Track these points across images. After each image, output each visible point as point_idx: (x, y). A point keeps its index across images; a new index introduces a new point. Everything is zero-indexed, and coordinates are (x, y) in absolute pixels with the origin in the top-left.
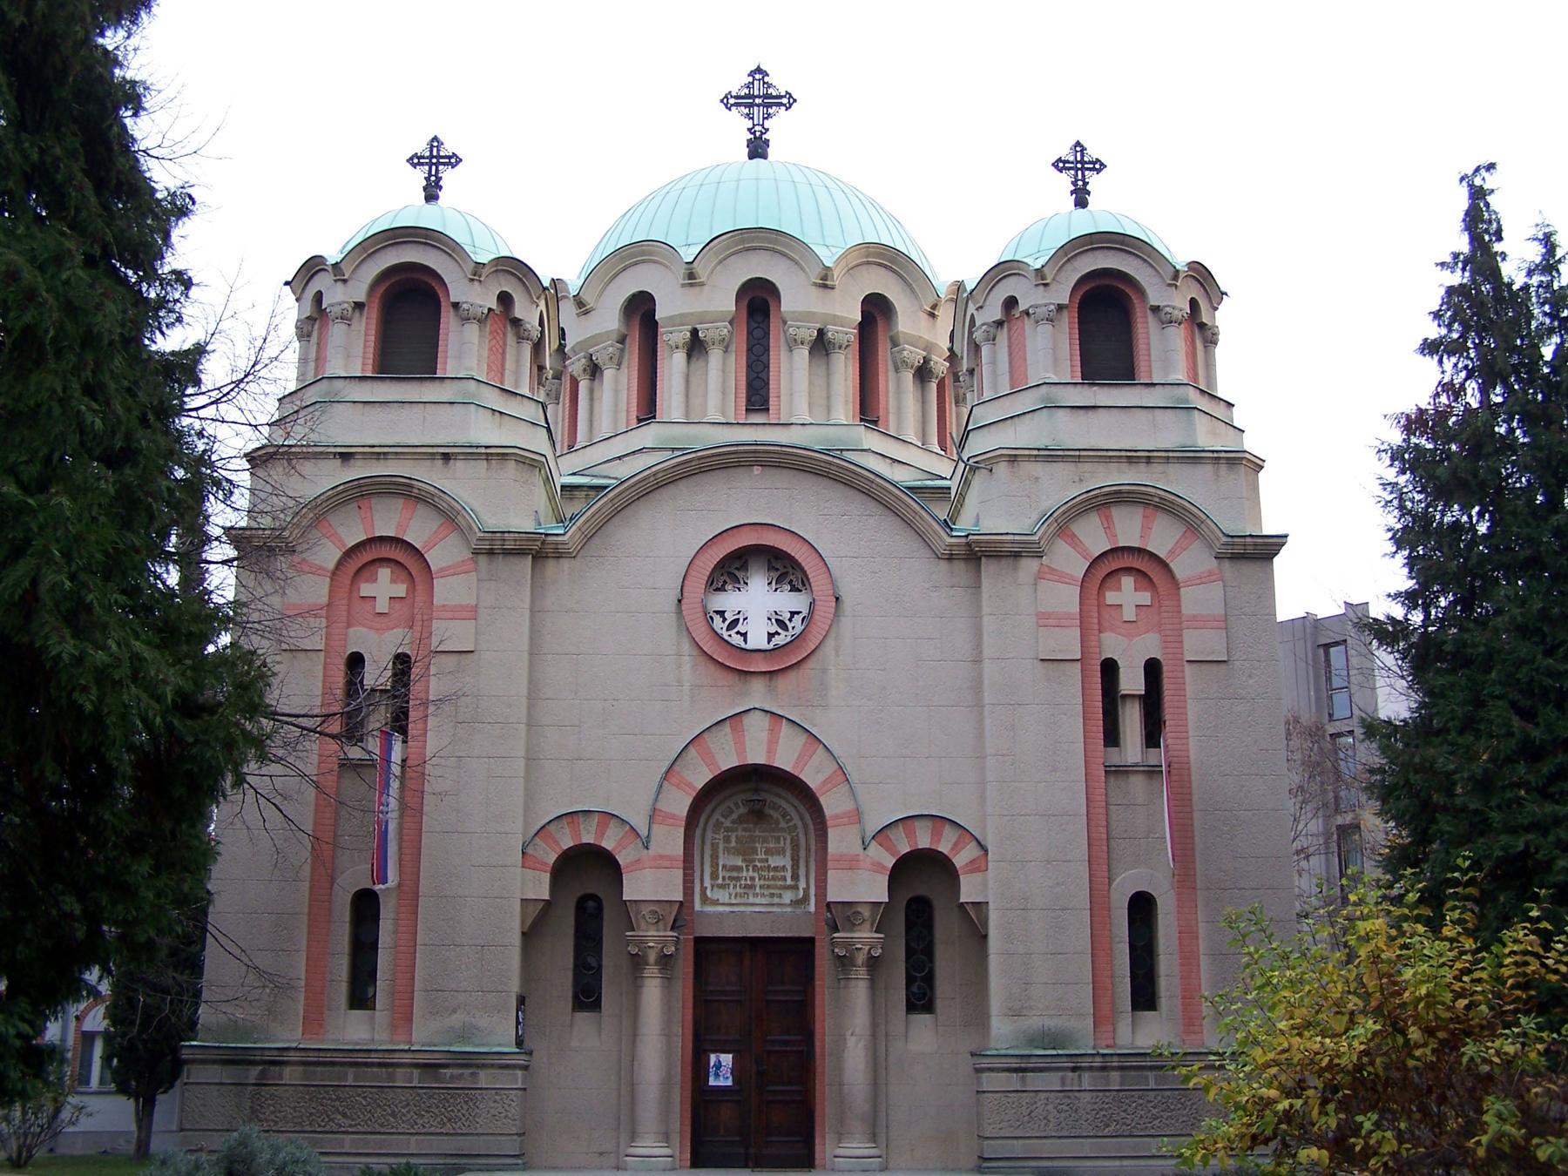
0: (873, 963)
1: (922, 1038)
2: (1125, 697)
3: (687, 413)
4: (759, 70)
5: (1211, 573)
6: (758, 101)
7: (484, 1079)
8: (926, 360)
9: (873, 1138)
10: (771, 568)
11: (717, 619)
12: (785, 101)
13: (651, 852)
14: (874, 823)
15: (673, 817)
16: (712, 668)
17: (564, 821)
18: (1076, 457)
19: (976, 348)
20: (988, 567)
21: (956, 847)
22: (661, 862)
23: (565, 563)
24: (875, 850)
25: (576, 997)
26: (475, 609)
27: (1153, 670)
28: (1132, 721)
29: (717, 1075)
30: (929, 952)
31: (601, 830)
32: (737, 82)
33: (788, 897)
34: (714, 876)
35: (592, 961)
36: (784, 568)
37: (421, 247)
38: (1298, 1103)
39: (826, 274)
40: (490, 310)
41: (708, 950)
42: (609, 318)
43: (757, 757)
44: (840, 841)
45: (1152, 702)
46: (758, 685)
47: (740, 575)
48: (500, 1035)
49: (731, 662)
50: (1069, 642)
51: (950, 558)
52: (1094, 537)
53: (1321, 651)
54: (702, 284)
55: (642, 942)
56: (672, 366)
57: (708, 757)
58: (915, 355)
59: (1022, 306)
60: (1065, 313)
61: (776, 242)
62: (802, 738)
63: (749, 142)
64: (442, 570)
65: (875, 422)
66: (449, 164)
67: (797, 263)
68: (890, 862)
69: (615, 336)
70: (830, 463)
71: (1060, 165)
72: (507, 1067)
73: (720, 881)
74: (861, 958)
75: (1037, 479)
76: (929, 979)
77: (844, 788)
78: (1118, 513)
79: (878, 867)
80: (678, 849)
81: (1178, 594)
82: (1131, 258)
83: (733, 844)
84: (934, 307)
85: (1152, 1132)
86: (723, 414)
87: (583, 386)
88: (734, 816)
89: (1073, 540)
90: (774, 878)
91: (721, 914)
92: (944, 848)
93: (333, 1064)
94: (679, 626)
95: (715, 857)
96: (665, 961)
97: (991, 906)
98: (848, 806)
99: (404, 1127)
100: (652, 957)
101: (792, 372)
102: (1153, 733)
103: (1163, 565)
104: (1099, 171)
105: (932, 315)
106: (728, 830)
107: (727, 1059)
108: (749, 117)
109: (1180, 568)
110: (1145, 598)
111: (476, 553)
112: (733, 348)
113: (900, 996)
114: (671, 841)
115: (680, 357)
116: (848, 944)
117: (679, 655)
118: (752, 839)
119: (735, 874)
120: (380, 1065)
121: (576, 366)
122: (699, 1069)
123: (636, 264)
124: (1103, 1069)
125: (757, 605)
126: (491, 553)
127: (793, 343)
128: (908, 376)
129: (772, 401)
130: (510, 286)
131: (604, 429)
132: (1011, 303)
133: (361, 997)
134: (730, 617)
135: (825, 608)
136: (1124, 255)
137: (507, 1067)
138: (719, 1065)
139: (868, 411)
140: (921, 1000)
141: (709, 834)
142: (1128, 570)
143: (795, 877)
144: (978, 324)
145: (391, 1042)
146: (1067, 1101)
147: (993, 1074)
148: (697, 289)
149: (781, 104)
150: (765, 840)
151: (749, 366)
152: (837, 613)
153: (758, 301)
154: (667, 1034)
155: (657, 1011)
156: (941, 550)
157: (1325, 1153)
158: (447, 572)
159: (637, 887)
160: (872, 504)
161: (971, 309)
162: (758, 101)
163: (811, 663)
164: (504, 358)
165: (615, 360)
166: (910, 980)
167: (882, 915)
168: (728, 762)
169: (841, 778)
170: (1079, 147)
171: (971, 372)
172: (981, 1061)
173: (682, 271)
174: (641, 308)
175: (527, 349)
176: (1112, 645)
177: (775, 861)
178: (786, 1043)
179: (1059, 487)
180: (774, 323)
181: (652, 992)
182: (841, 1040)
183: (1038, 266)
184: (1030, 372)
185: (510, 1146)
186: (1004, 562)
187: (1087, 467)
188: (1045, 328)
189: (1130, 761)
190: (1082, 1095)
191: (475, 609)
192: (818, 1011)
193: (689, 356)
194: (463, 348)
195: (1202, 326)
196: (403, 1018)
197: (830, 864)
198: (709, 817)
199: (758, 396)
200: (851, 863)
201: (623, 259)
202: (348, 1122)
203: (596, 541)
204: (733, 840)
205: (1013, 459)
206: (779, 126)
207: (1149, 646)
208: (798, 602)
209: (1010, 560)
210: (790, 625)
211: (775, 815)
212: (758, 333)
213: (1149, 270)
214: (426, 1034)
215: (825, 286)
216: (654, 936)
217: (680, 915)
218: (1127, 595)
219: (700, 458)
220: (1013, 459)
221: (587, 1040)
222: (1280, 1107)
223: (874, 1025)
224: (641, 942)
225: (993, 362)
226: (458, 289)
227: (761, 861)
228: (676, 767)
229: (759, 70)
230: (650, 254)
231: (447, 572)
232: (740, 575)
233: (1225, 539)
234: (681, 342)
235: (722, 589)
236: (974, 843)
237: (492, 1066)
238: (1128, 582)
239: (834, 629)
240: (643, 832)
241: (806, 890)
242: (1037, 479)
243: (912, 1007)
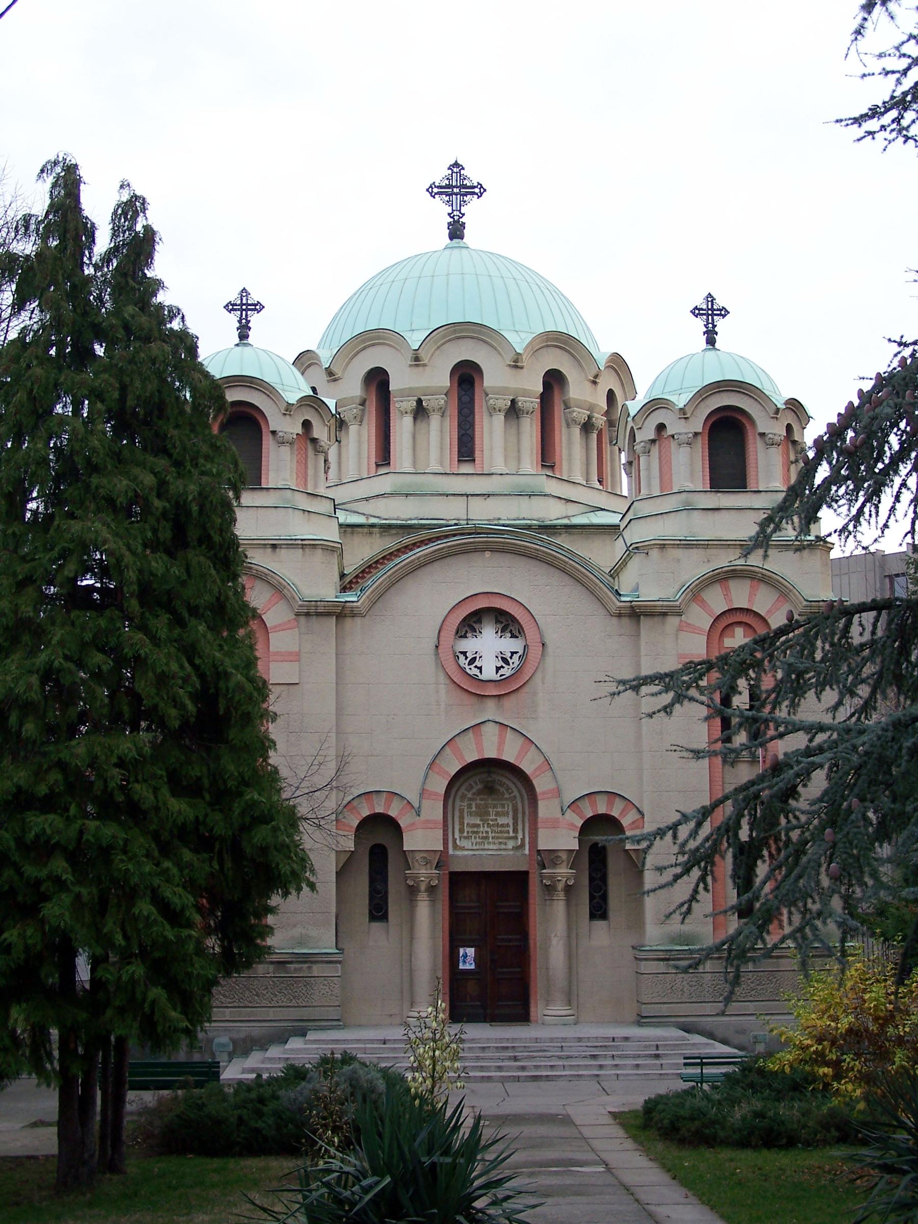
0: (568, 889)
1: (600, 936)
4: (456, 164)
6: (455, 190)
7: (317, 970)
8: (590, 417)
9: (569, 1003)
11: (462, 657)
12: (477, 190)
13: (422, 818)
14: (569, 798)
15: (436, 794)
16: (459, 692)
20: (645, 622)
21: (624, 812)
22: (428, 825)
23: (358, 620)
24: (570, 815)
25: (370, 912)
26: (298, 654)
29: (464, 962)
30: (604, 879)
31: (388, 804)
32: (439, 174)
33: (511, 844)
34: (461, 831)
36: (507, 622)
37: (248, 389)
38: (820, 1047)
39: (517, 358)
41: (459, 881)
43: (491, 753)
44: (546, 809)
46: (491, 704)
47: (476, 626)
48: (326, 943)
49: (472, 688)
51: (620, 616)
52: (717, 600)
53: (887, 580)
54: (425, 365)
55: (416, 877)
56: (402, 426)
57: (458, 754)
58: (581, 415)
59: (670, 431)
60: (699, 438)
61: (480, 332)
62: (521, 740)
63: (449, 224)
64: (275, 627)
66: (255, 309)
67: (495, 349)
68: (579, 823)
69: (358, 401)
70: (538, 550)
72: (331, 962)
73: (465, 834)
74: (560, 886)
75: (679, 560)
76: (605, 897)
77: (549, 774)
78: (732, 584)
79: (572, 826)
82: (746, 398)
83: (474, 809)
84: (596, 376)
85: (751, 999)
86: (442, 465)
88: (474, 790)
89: (703, 604)
90: (501, 832)
91: (466, 856)
92: (615, 813)
94: (437, 664)
95: (462, 818)
96: (431, 889)
98: (553, 786)
99: (265, 1003)
100: (423, 887)
101: (491, 431)
104: (724, 316)
105: (594, 383)
106: (470, 799)
107: (471, 951)
111: (298, 615)
112: (448, 413)
113: (585, 910)
114: (434, 810)
115: (408, 420)
116: (552, 877)
117: (437, 683)
118: (486, 806)
119: (475, 829)
122: (453, 958)
123: (373, 345)
125: (489, 646)
126: (307, 614)
127: (492, 411)
128: (576, 431)
129: (477, 454)
130: (310, 415)
131: (351, 472)
132: (661, 427)
135: (535, 651)
136: (742, 396)
137: (331, 962)
138: (465, 956)
139: (547, 457)
140: (599, 911)
141: (458, 803)
142: (739, 623)
143: (515, 830)
146: (695, 979)
147: (648, 962)
148: (421, 369)
149: (474, 193)
150: (495, 806)
151: (459, 425)
152: (543, 654)
153: (466, 376)
154: (433, 937)
155: (427, 921)
157: (831, 1070)
158: (278, 628)
160: (567, 578)
162: (455, 190)
163: (526, 689)
164: (306, 468)
165: (358, 419)
166: (592, 898)
167: (574, 858)
170: (710, 298)
172: (639, 952)
173: (410, 355)
177: (502, 820)
178: (510, 940)
179: (695, 567)
181: (423, 909)
182: (547, 940)
183: (681, 406)
184: (675, 479)
186: (656, 619)
187: (714, 551)
188: (685, 449)
190: (706, 975)
191: (298, 654)
192: (531, 920)
195: (794, 442)
197: (539, 825)
198: (457, 791)
200: (554, 824)
201: (364, 341)
202: (228, 1000)
203: (379, 605)
204: (474, 806)
205: (663, 547)
206: (473, 210)
208: (516, 645)
210: (511, 661)
211: (502, 790)
212: (466, 399)
215: (516, 367)
216: (424, 873)
217: (441, 860)
219: (449, 547)
220: (663, 547)
221: (379, 941)
222: (812, 1049)
223: (569, 928)
224: (415, 878)
225: (648, 469)
227: (492, 820)
228: (437, 761)
229: (456, 164)
230: (384, 338)
231: (278, 628)
232: (476, 626)
233: (805, 603)
234: (409, 409)
235: (465, 636)
236: (635, 810)
237: (322, 962)
239: (541, 665)
240: (416, 805)
241: (523, 840)
242: (679, 560)
243: (593, 916)
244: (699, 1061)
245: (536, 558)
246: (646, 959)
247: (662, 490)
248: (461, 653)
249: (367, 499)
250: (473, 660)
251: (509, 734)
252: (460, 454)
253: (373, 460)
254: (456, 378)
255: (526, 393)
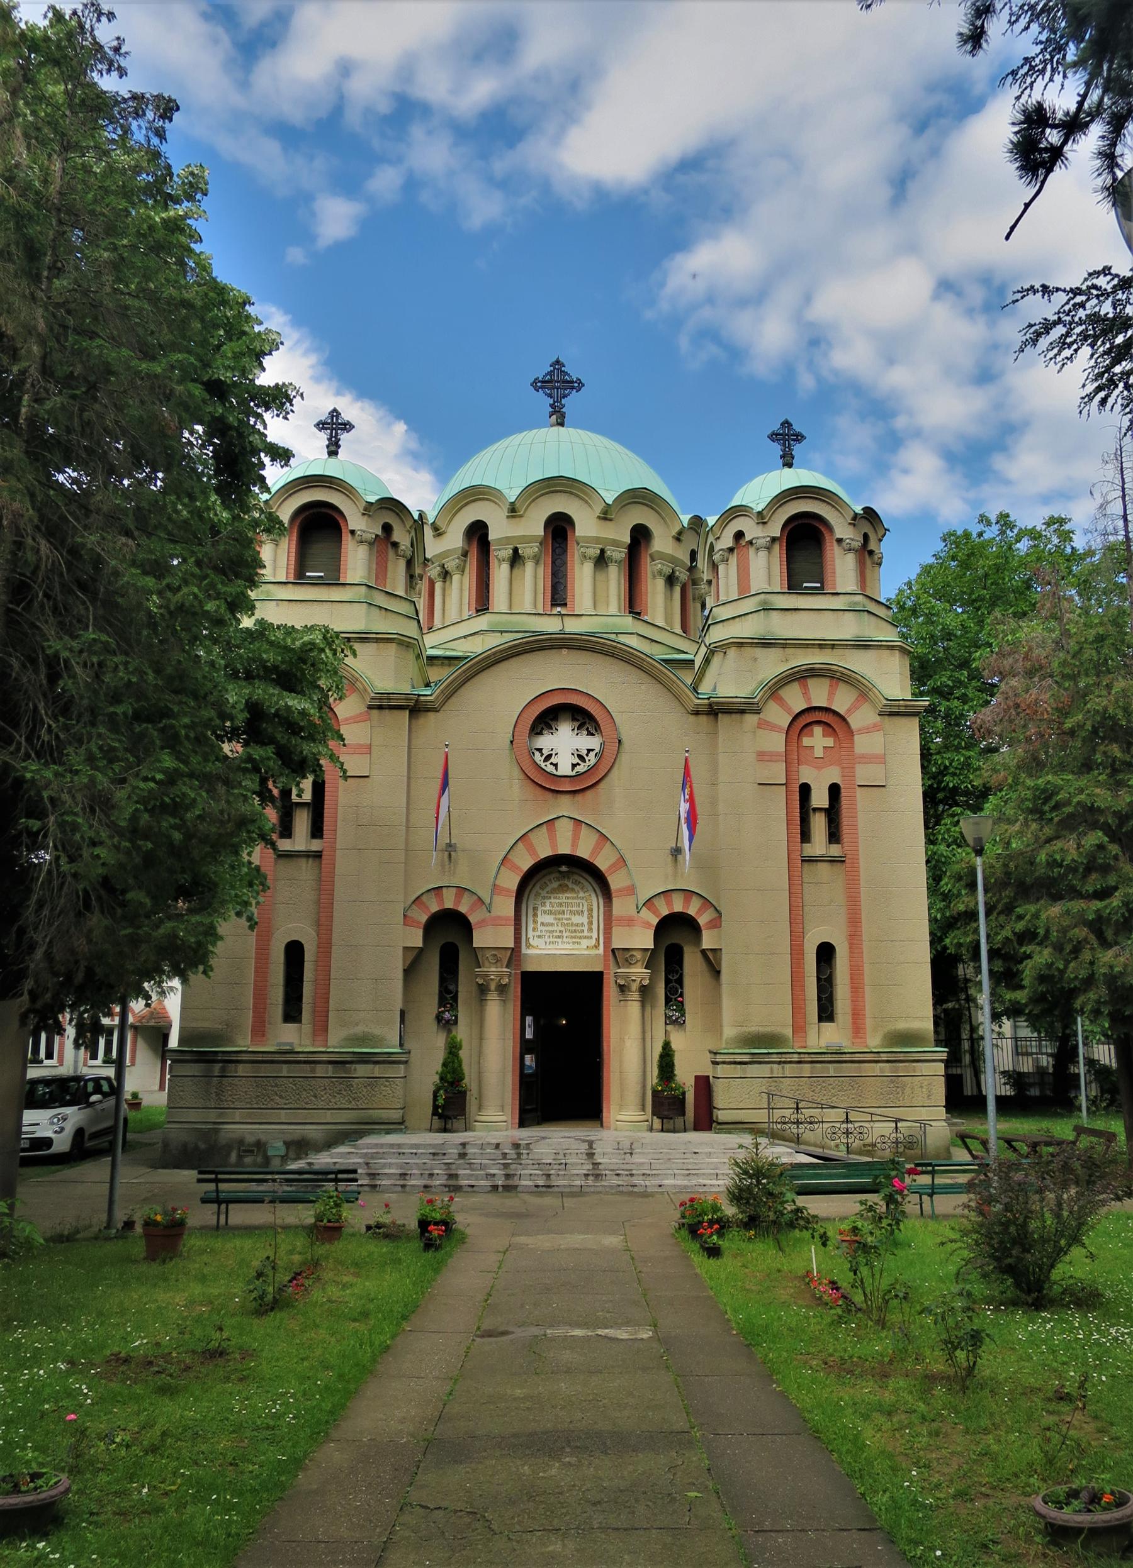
0: (644, 991)
2: (815, 810)
3: (510, 607)
4: (558, 362)
5: (875, 725)
10: (574, 719)
11: (537, 754)
15: (508, 890)
17: (433, 893)
18: (784, 644)
19: (714, 567)
23: (431, 715)
24: (645, 914)
26: (369, 747)
27: (834, 791)
28: (819, 824)
32: (542, 370)
35: (452, 987)
36: (584, 718)
40: (377, 536)
42: (455, 538)
43: (564, 849)
44: (620, 907)
45: (833, 813)
46: (565, 800)
49: (546, 784)
50: (778, 772)
51: (697, 713)
52: (796, 699)
55: (487, 976)
56: (500, 573)
57: (531, 849)
59: (748, 538)
60: (777, 547)
61: (572, 487)
64: (347, 719)
65: (639, 614)
67: (587, 502)
68: (655, 921)
71: (774, 437)
74: (635, 986)
78: (811, 682)
79: (647, 924)
80: (511, 912)
81: (853, 743)
87: (438, 586)
89: (781, 701)
93: (272, 1062)
95: (535, 915)
97: (724, 951)
98: (613, 859)
99: (321, 1104)
100: (493, 986)
101: (582, 576)
102: (834, 836)
103: (843, 719)
108: (550, 396)
109: (855, 721)
110: (830, 742)
114: (506, 907)
115: (505, 567)
116: (627, 976)
120: (305, 1062)
121: (434, 571)
123: (474, 501)
124: (799, 1062)
125: (565, 745)
126: (380, 707)
131: (453, 615)
132: (739, 535)
133: (292, 1013)
134: (546, 753)
139: (633, 605)
142: (818, 723)
143: (590, 929)
144: (716, 550)
145: (313, 1045)
153: (559, 529)
156: (691, 708)
159: (481, 939)
160: (644, 675)
161: (711, 539)
163: (602, 785)
168: (545, 852)
169: (622, 864)
170: (786, 424)
171: (709, 582)
174: (478, 532)
175: (402, 564)
176: (806, 775)
177: (576, 919)
179: (773, 665)
180: (571, 544)
185: (395, 1115)
186: (734, 716)
189: (818, 853)
191: (369, 747)
193: (512, 566)
194: (356, 561)
195: (871, 553)
196: (321, 1028)
199: (558, 595)
200: (629, 922)
201: (465, 497)
207: (833, 775)
208: (594, 742)
209: (738, 716)
213: (836, 513)
214: (336, 1041)
215: (606, 519)
216: (494, 971)
218: (818, 740)
224: (485, 976)
226: (355, 520)
229: (558, 362)
232: (553, 724)
233: (886, 702)
235: (541, 733)
238: (818, 730)
240: (487, 901)
241: (598, 940)
242: (756, 659)
244: (213, 1176)
245: (613, 656)
246: (724, 1063)
247: (739, 594)
248: (537, 749)
249: (464, 637)
250: (549, 757)
251: (584, 830)
252: (553, 599)
253: (474, 606)
254: (550, 530)
255: (615, 543)
